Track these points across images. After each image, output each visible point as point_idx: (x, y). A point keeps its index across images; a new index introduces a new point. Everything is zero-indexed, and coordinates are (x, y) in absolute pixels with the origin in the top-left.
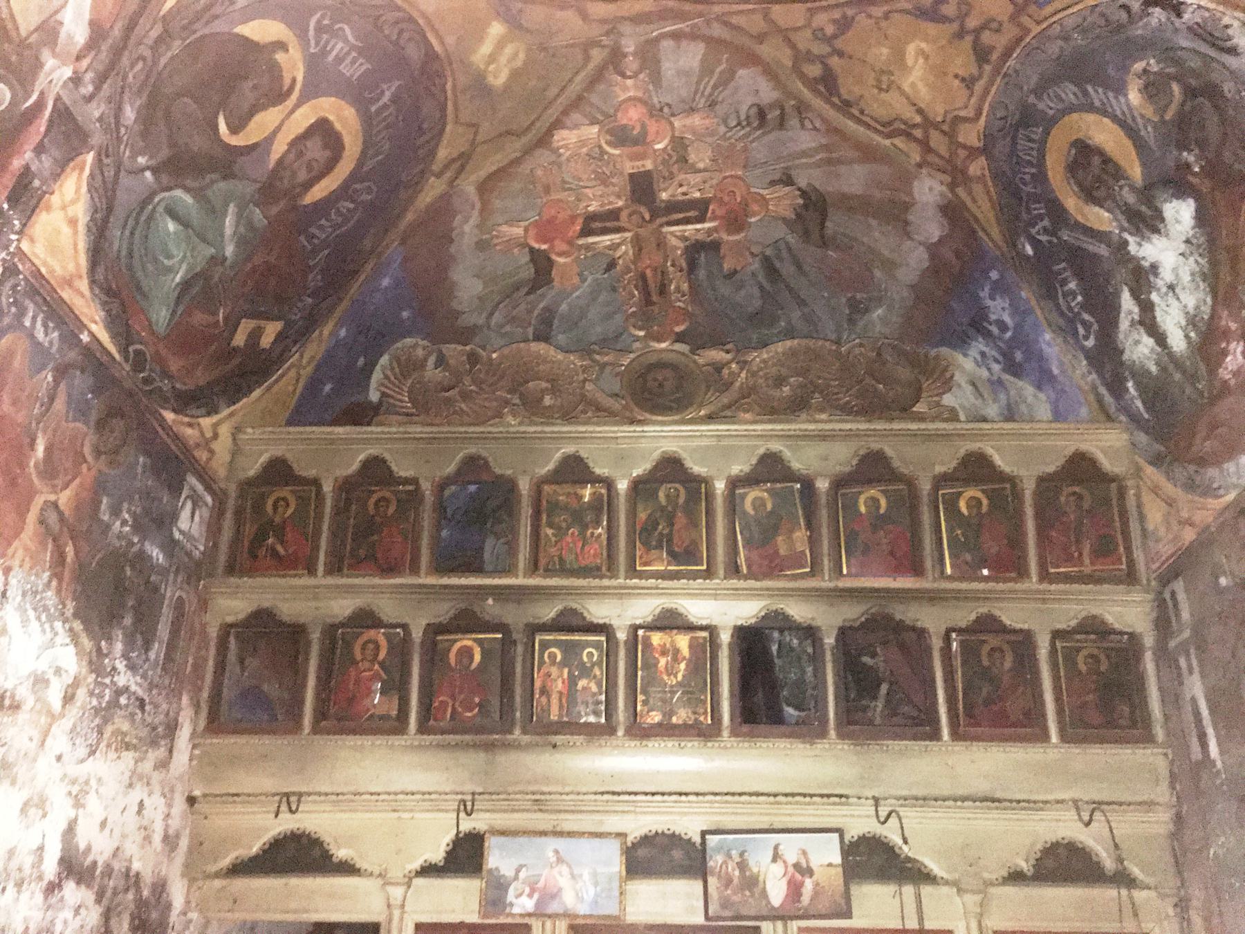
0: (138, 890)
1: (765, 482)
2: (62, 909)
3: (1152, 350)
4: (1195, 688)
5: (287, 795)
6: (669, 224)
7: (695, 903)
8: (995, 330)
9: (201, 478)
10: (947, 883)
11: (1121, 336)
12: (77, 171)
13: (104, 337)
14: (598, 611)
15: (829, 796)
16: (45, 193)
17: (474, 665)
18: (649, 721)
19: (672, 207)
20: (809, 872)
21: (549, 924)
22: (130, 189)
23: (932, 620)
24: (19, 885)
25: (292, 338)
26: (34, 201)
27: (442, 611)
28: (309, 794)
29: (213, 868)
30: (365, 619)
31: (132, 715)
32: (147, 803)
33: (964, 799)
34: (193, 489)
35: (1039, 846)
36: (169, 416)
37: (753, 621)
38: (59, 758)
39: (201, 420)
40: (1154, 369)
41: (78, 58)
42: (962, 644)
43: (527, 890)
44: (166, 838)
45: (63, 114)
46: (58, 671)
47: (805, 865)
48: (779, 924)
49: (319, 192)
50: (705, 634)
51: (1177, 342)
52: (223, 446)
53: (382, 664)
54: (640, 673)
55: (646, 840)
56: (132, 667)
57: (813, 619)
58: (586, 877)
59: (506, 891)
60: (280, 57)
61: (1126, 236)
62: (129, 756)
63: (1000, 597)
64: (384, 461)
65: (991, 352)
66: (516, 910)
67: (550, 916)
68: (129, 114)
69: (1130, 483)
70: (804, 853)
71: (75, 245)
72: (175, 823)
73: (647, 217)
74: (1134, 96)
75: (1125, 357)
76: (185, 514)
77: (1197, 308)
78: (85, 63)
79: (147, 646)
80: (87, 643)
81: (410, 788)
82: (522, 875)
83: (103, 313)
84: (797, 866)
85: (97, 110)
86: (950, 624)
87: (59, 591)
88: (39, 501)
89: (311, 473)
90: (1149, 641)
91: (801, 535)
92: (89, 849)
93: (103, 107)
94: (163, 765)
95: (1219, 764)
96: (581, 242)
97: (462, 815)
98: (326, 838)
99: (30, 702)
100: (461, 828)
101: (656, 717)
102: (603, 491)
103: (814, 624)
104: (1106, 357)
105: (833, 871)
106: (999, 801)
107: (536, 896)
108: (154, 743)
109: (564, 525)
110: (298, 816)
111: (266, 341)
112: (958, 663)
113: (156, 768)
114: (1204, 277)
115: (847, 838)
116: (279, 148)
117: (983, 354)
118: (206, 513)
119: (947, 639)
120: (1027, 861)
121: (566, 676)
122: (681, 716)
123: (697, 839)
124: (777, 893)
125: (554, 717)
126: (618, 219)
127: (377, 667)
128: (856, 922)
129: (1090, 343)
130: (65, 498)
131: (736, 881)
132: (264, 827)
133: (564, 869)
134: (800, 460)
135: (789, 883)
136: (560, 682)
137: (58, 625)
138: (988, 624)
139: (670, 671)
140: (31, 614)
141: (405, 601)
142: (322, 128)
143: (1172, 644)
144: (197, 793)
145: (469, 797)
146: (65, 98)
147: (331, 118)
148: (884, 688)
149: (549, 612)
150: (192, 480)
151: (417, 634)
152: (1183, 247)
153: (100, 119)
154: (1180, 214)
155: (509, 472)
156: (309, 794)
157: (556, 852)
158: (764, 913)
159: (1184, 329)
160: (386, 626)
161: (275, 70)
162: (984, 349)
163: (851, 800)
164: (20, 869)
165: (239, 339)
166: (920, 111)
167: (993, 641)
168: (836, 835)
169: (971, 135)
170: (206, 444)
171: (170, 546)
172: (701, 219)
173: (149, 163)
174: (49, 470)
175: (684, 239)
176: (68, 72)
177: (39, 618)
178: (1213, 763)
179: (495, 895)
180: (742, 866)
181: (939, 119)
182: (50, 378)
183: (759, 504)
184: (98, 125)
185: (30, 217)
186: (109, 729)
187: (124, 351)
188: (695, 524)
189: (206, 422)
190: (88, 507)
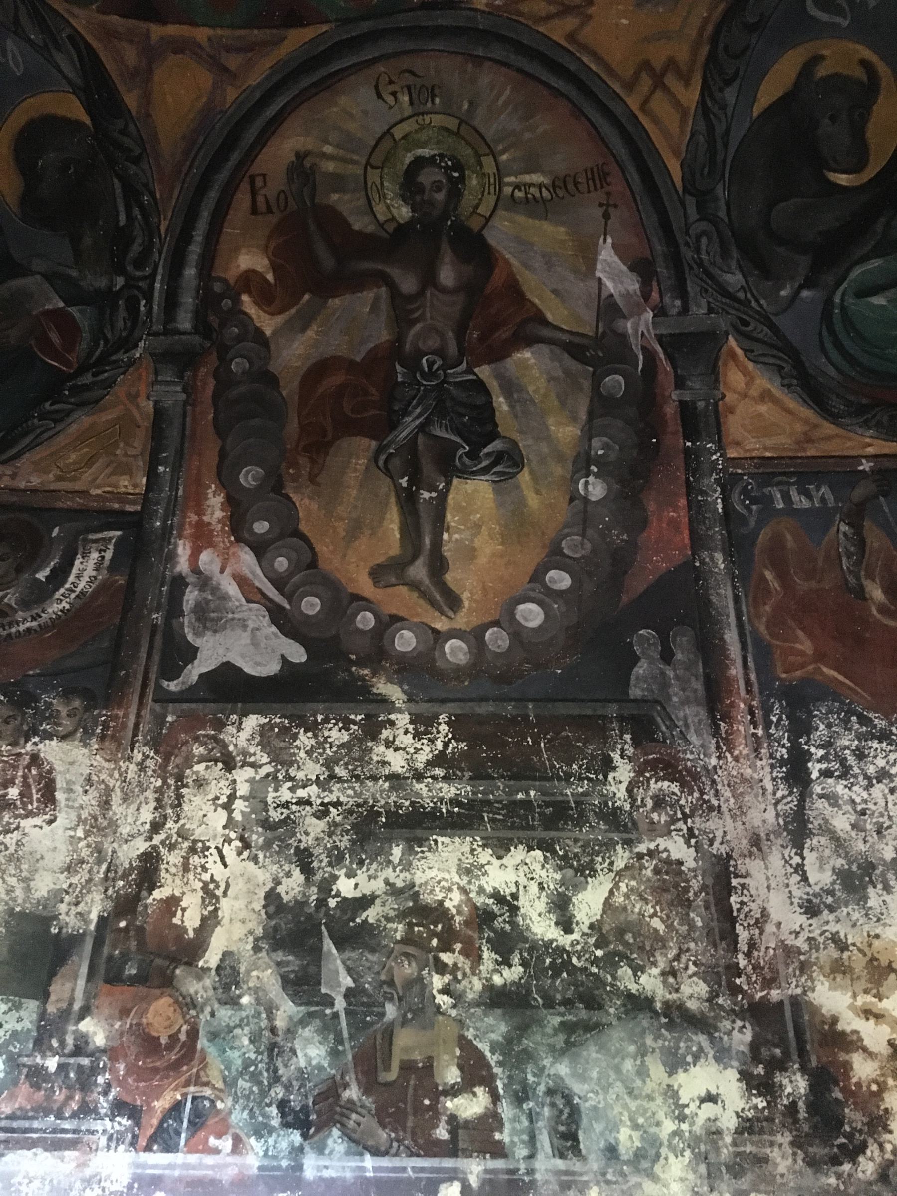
12: (731, 363)
16: (716, 404)
26: (712, 420)
45: (671, 343)
68: (734, 279)
78: (655, 295)
146: (664, 332)
161: (837, 82)
173: (796, 285)
185: (719, 432)
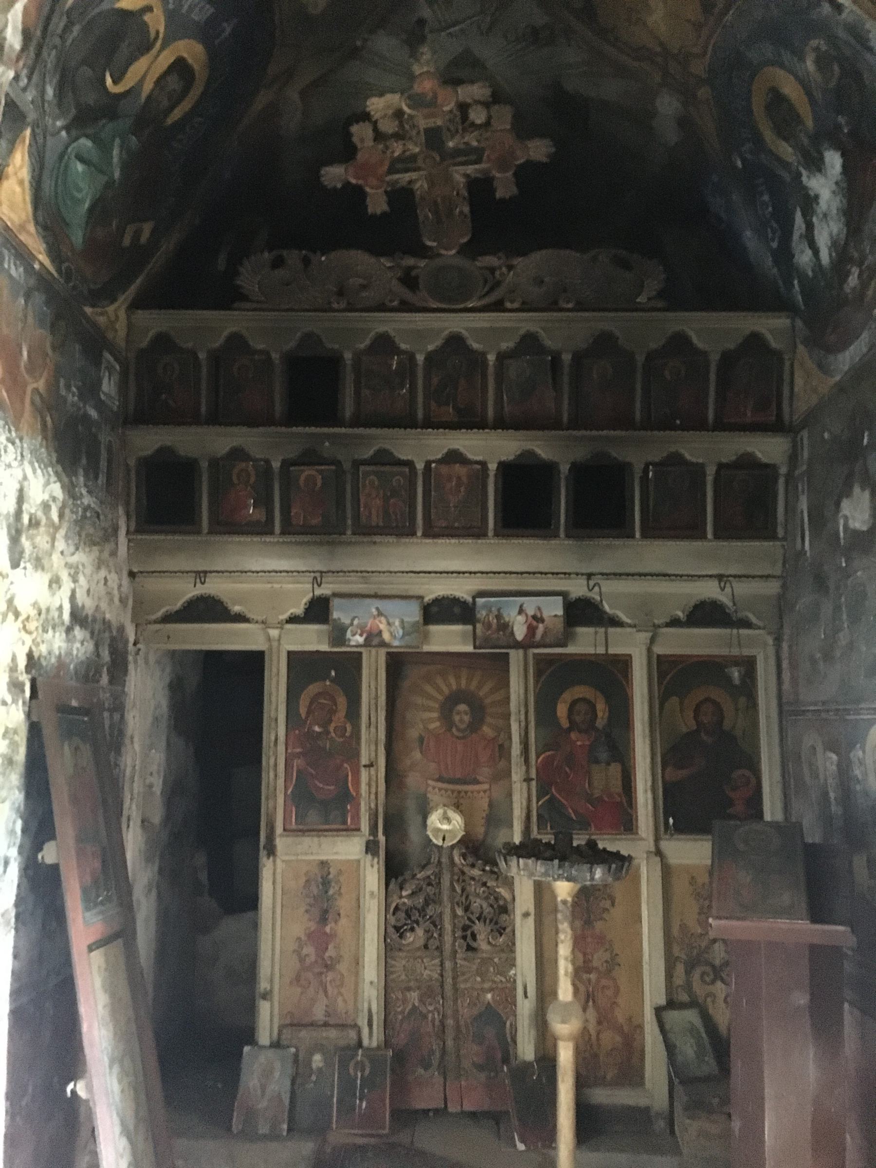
0: (111, 632)
4: (803, 505)
6: (455, 165)
10: (630, 626)
11: (794, 244)
13: (47, 262)
17: (317, 488)
19: (457, 152)
20: (541, 620)
22: (53, 145)
24: (54, 628)
27: (292, 451)
28: (211, 572)
30: (238, 454)
31: (95, 523)
32: (108, 578)
33: (658, 575)
34: (109, 362)
35: (692, 604)
36: (88, 310)
37: (511, 458)
38: (62, 553)
39: (107, 309)
40: (810, 274)
41: (18, 60)
42: (655, 473)
43: (359, 631)
44: (121, 601)
46: (54, 499)
47: (539, 615)
49: (177, 114)
51: (825, 257)
52: (121, 326)
55: (437, 601)
58: (397, 623)
59: (346, 632)
60: (147, 17)
61: (801, 169)
62: (95, 548)
64: (241, 336)
66: (352, 643)
69: (786, 357)
70: (539, 609)
71: (24, 199)
72: (124, 589)
73: (438, 159)
74: (810, 64)
76: (105, 381)
77: (838, 235)
78: (21, 63)
80: (66, 480)
81: (278, 569)
82: (356, 622)
83: (44, 246)
84: (534, 617)
85: (29, 96)
87: (47, 448)
88: (29, 389)
92: (83, 606)
93: (34, 92)
95: (808, 554)
96: (388, 178)
97: (315, 585)
98: (224, 599)
99: (44, 521)
100: (316, 593)
110: (206, 585)
111: (144, 239)
112: (651, 488)
114: (845, 214)
116: (148, 86)
119: (646, 471)
120: (683, 612)
124: (520, 633)
126: (415, 161)
130: (41, 384)
133: (383, 619)
138: (676, 459)
142: (180, 66)
143: (797, 472)
144: (135, 570)
147: (185, 55)
150: (107, 355)
151: (276, 465)
152: (834, 187)
153: (32, 102)
154: (834, 160)
155: (336, 346)
156: (211, 572)
157: (377, 609)
159: (830, 249)
163: (572, 576)
164: (53, 619)
165: (127, 241)
166: (661, 44)
168: (561, 598)
169: (698, 68)
171: (100, 406)
172: (478, 161)
175: (467, 176)
176: (11, 74)
179: (339, 635)
180: (499, 617)
181: (676, 51)
182: (23, 302)
184: (31, 106)
187: (59, 271)
189: (111, 309)
190: (53, 386)
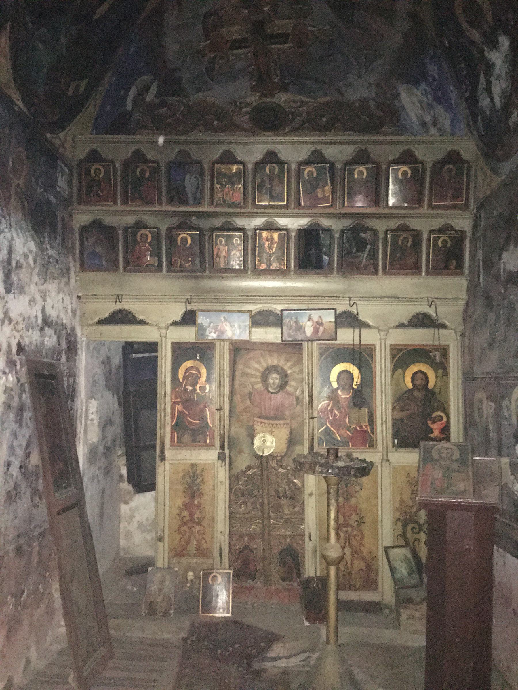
1: (314, 164)
2: (46, 337)
3: (489, 104)
5: (118, 296)
7: (278, 335)
8: (430, 79)
9: (63, 162)
14: (240, 222)
15: (331, 297)
18: (261, 268)
19: (272, 36)
21: (222, 343)
23: (380, 226)
24: (32, 328)
25: (90, 88)
27: (175, 221)
29: (90, 322)
30: (140, 225)
32: (64, 298)
36: (48, 135)
43: (213, 331)
48: (310, 342)
50: (285, 232)
53: (150, 244)
54: (257, 248)
56: (52, 247)
57: (331, 226)
58: (236, 326)
62: (57, 281)
63: (411, 216)
65: (428, 89)
66: (210, 338)
67: (223, 340)
70: (320, 317)
75: (480, 104)
79: (56, 238)
82: (212, 325)
84: (317, 323)
86: (388, 228)
89: (110, 157)
90: (469, 234)
91: (328, 188)
94: (67, 283)
95: (482, 285)
97: (188, 304)
101: (264, 266)
102: (241, 167)
103: (331, 228)
104: (472, 102)
105: (331, 324)
106: (399, 298)
107: (217, 333)
108: (63, 276)
109: (224, 183)
113: (65, 285)
115: (338, 312)
117: (425, 90)
118: (66, 177)
121: (226, 250)
122: (275, 266)
123: (279, 313)
124: (309, 331)
125: (222, 266)
127: (147, 245)
128: (338, 342)
129: (467, 94)
130: (21, 182)
131: (294, 328)
132: (108, 308)
134: (330, 152)
135: (314, 328)
136: (224, 252)
137: (27, 233)
139: (270, 247)
140: (19, 231)
141: (157, 216)
144: (80, 294)
145: (189, 297)
148: (369, 247)
149: (218, 222)
150: (60, 163)
154: (504, 42)
157: (224, 317)
158: (304, 338)
160: (151, 228)
162: (426, 88)
163: (340, 298)
165: (70, 93)
167: (404, 235)
168: (334, 311)
170: (62, 145)
171: (57, 195)
172: (285, 42)
174: (15, 171)
177: (21, 232)
178: (480, 283)
180: (296, 322)
183: (310, 173)
186: (49, 272)
187: (29, 110)
188: (282, 183)
